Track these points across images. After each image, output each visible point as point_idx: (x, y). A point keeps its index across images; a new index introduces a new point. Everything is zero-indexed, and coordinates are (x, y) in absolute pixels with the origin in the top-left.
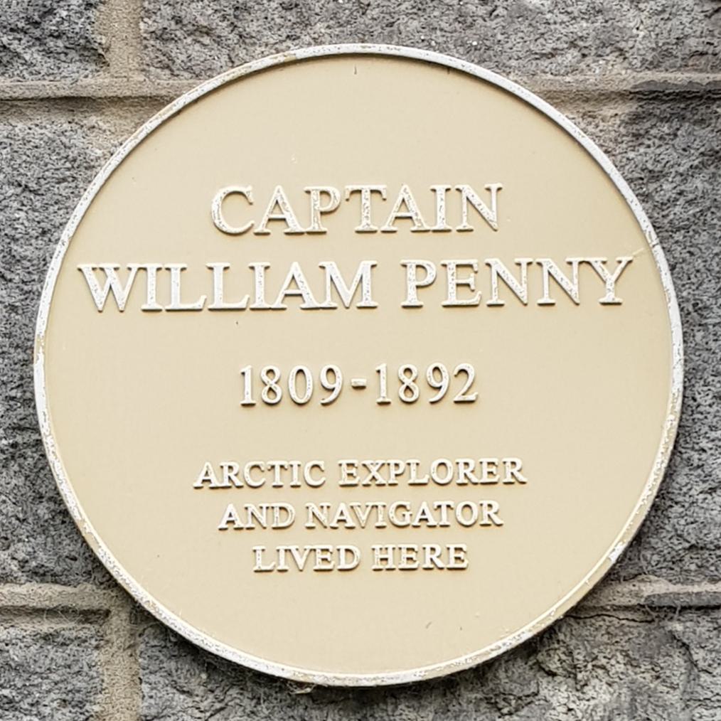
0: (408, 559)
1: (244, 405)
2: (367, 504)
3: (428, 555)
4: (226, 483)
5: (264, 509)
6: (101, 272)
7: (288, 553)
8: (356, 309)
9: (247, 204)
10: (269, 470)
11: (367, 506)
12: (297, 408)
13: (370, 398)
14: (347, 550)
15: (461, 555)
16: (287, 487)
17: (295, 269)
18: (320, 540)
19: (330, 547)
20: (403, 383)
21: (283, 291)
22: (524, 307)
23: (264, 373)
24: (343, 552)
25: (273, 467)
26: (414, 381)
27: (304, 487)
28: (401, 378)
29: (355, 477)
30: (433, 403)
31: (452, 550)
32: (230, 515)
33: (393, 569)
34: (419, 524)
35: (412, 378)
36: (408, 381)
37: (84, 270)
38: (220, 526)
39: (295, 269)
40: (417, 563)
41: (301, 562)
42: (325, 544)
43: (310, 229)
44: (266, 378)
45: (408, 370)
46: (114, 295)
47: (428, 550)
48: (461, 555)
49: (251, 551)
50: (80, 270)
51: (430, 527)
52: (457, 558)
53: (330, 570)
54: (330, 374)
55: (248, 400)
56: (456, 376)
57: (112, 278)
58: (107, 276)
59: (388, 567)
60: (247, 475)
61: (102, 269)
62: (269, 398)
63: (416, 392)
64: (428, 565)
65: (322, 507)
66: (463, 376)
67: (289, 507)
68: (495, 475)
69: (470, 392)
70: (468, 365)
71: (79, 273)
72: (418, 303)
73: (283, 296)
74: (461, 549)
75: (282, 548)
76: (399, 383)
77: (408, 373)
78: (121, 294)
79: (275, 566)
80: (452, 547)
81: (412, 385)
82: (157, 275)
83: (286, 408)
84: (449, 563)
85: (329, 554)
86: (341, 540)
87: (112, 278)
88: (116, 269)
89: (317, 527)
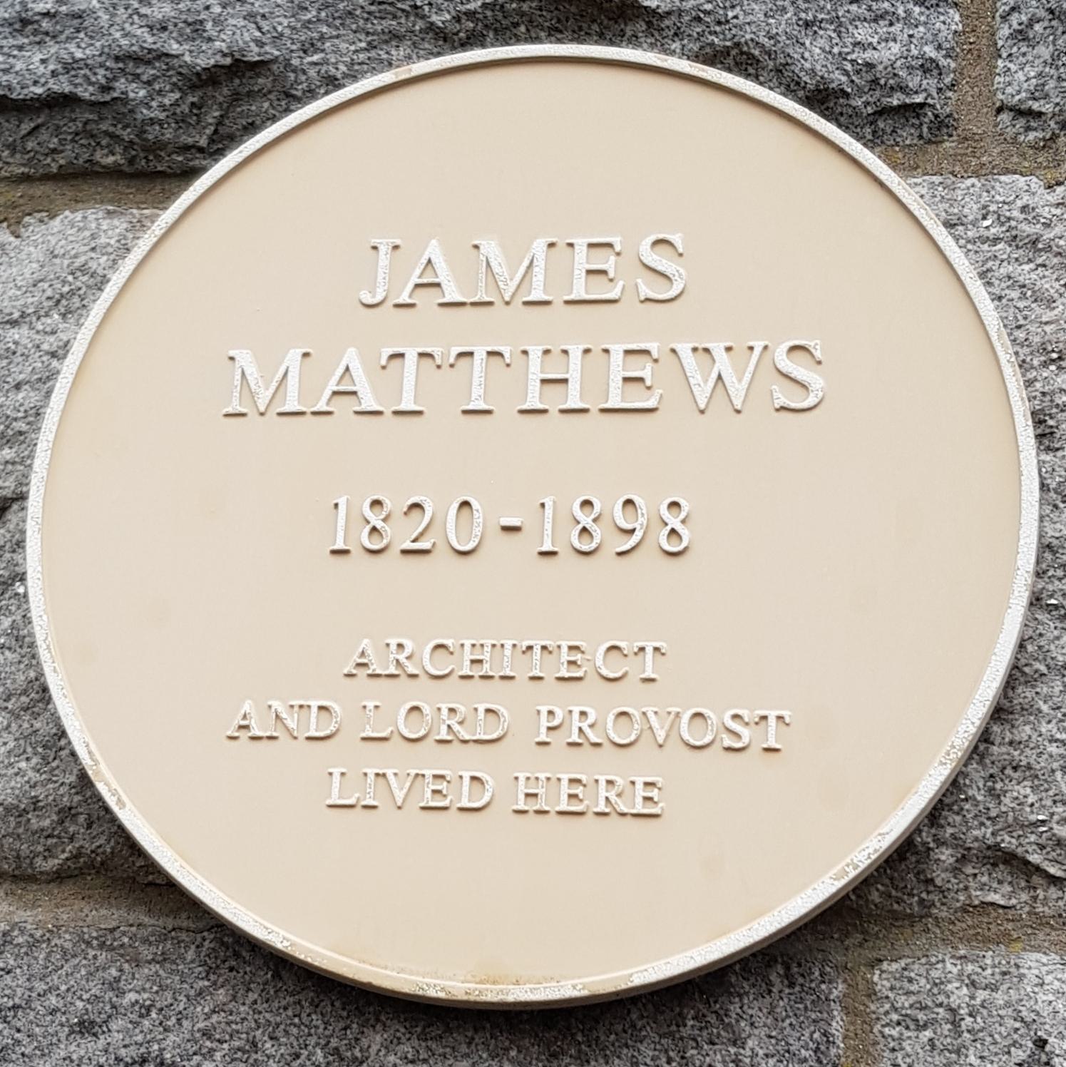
0: (435, 792)
1: (334, 552)
2: (669, 709)
3: (603, 791)
4: (392, 670)
5: (296, 709)
6: (706, 356)
7: (381, 780)
8: (275, 416)
9: (676, 254)
10: (636, 654)
11: (669, 713)
12: (463, 560)
13: (525, 546)
14: (474, 778)
15: (654, 793)
16: (634, 677)
17: (351, 357)
18: (430, 761)
19: (584, 778)
20: (368, 522)
21: (332, 386)
22: (734, 414)
23: (664, 507)
24: (466, 781)
25: (642, 649)
26: (595, 520)
27: (423, 678)
28: (664, 518)
29: (579, 666)
30: (620, 554)
31: (639, 786)
32: (245, 717)
33: (546, 812)
34: (236, 734)
35: (593, 516)
36: (586, 520)
37: (680, 353)
38: (229, 733)
39: (351, 357)
40: (449, 798)
41: (399, 796)
42: (441, 769)
43: (476, 299)
44: (666, 515)
45: (674, 505)
46: (724, 385)
47: (603, 784)
48: (654, 793)
49: (512, 778)
50: (673, 351)
51: (254, 738)
52: (648, 799)
53: (445, 808)
54: (630, 508)
55: (340, 545)
56: (405, 513)
57: (723, 362)
58: (714, 361)
59: (537, 807)
60: (599, 662)
61: (707, 350)
62: (580, 542)
63: (597, 540)
64: (602, 807)
65: (292, 706)
66: (416, 513)
67: (502, 710)
68: (579, 666)
69: (423, 538)
70: (423, 498)
71: (672, 355)
72: (540, 406)
73: (330, 392)
74: (578, 781)
75: (371, 772)
76: (364, 522)
77: (675, 510)
78: (737, 389)
79: (358, 799)
80: (565, 777)
81: (679, 528)
82: (302, 362)
83: (442, 559)
84: (634, 807)
85: (445, 783)
86: (461, 764)
87: (723, 362)
88: (729, 349)
89: (281, 738)
